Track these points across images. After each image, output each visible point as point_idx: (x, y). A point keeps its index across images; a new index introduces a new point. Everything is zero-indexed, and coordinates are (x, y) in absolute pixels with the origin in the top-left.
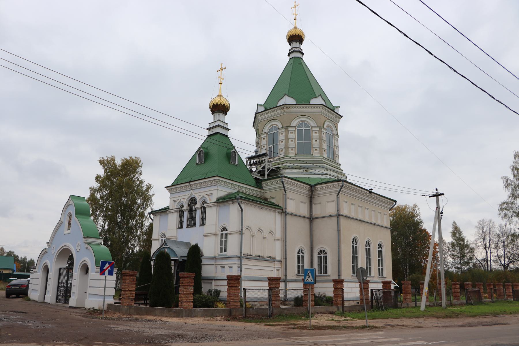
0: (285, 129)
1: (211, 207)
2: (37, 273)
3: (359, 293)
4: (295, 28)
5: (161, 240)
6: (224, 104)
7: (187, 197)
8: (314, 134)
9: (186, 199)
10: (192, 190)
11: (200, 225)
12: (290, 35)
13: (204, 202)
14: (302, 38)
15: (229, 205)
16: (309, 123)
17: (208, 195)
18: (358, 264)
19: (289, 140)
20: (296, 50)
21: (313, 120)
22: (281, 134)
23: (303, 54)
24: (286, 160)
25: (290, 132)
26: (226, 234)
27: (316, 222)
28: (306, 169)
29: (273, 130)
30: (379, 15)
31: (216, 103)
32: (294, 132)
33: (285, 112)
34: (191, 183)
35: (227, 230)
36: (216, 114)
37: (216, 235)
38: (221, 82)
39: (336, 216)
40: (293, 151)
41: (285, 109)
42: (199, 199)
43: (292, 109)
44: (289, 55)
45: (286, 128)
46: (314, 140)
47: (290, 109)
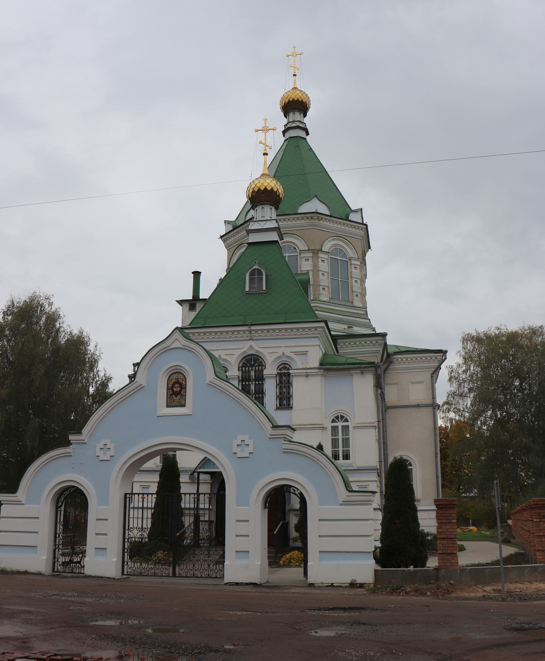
0: (313, 253)
1: (307, 376)
2: (23, 504)
3: (420, 525)
4: (295, 88)
6: (272, 189)
7: (238, 353)
8: (353, 270)
9: (235, 357)
10: (252, 340)
11: (276, 408)
12: (289, 100)
13: (283, 366)
14: (308, 106)
15: (352, 375)
16: (347, 251)
17: (297, 353)
18: (413, 482)
19: (320, 272)
20: (294, 125)
21: (352, 247)
22: (303, 260)
23: (307, 134)
24: (316, 306)
25: (320, 260)
26: (346, 429)
27: (391, 415)
28: (349, 325)
29: (286, 252)
31: (264, 187)
32: (326, 261)
33: (314, 225)
34: (253, 328)
35: (347, 420)
36: (257, 208)
37: (323, 428)
38: (265, 152)
39: (432, 406)
40: (326, 292)
41: (315, 221)
42: (272, 359)
43: (325, 223)
44: (284, 132)
45: (316, 252)
46: (354, 280)
47: (321, 222)
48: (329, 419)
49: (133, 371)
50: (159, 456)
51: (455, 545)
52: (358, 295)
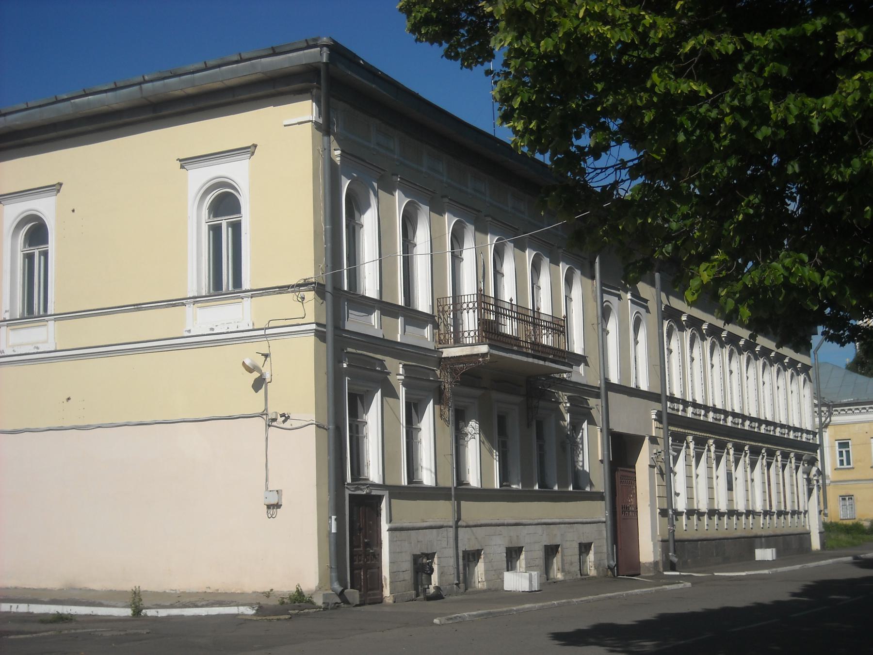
5: (281, 417)
30: (176, 340)
50: (822, 246)
51: (619, 173)
52: (416, 558)
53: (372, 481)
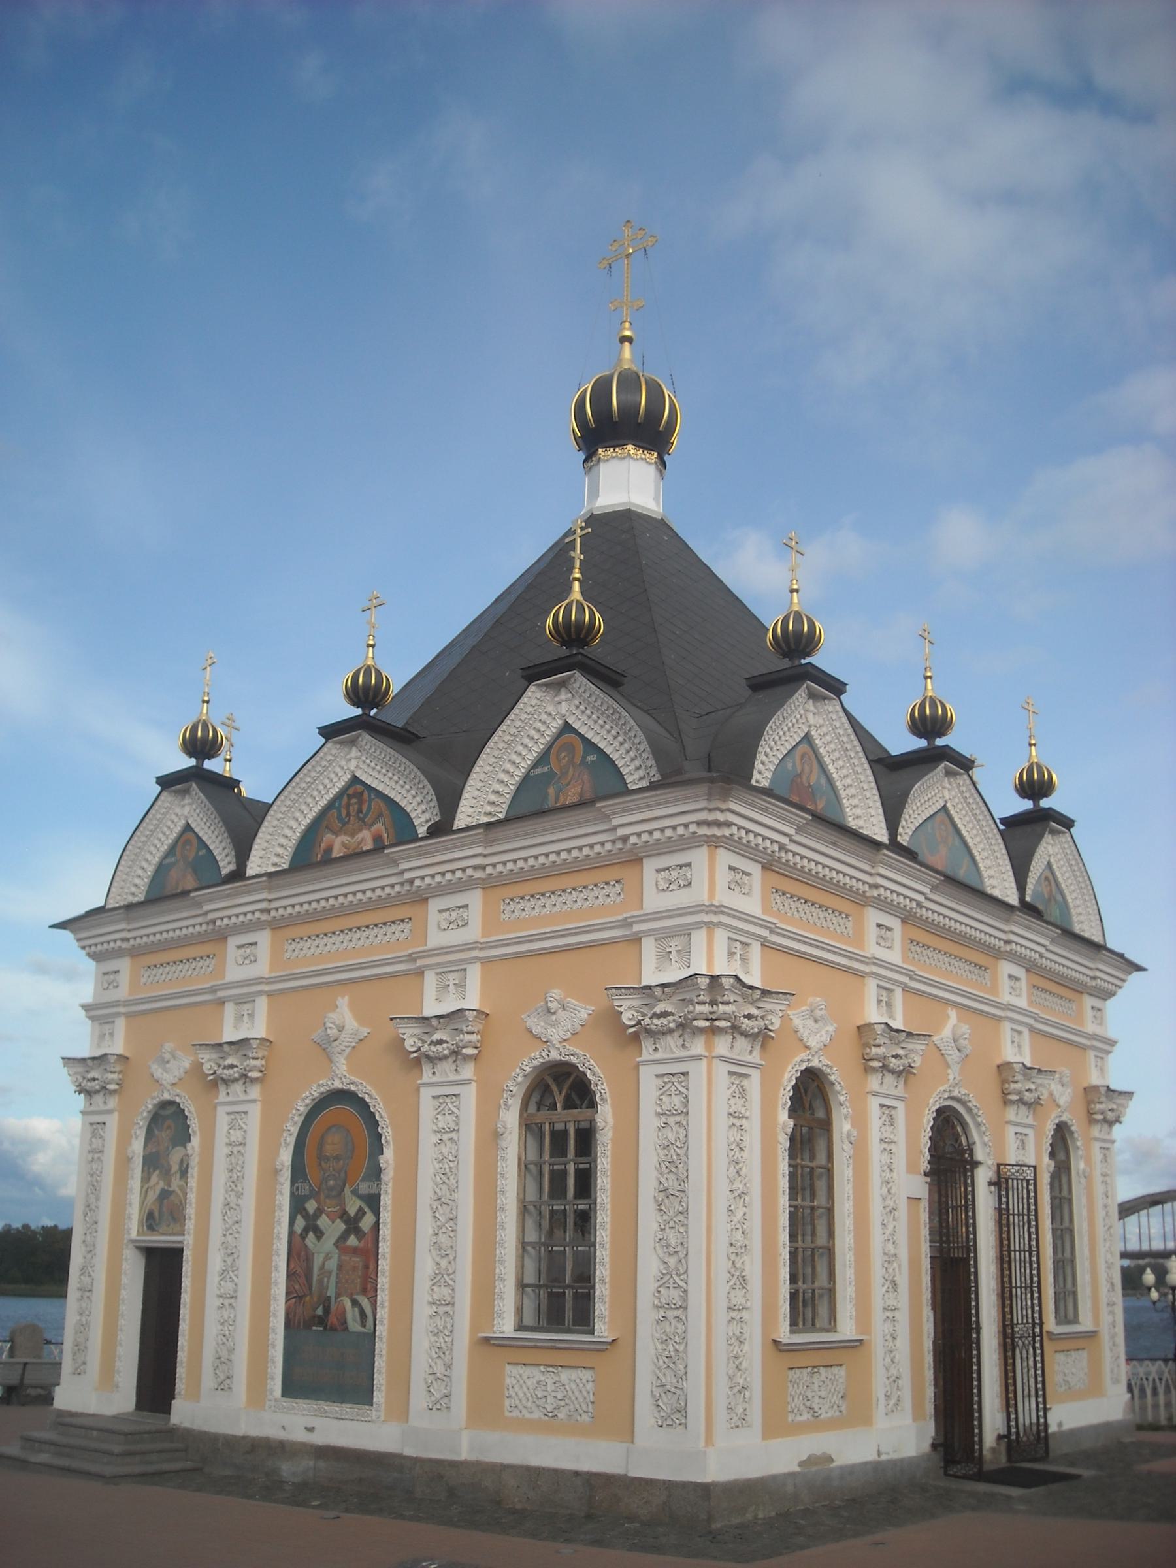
48: (143, 1475)
49: (1068, 823)
50: (352, 1215)
53: (174, 1425)
